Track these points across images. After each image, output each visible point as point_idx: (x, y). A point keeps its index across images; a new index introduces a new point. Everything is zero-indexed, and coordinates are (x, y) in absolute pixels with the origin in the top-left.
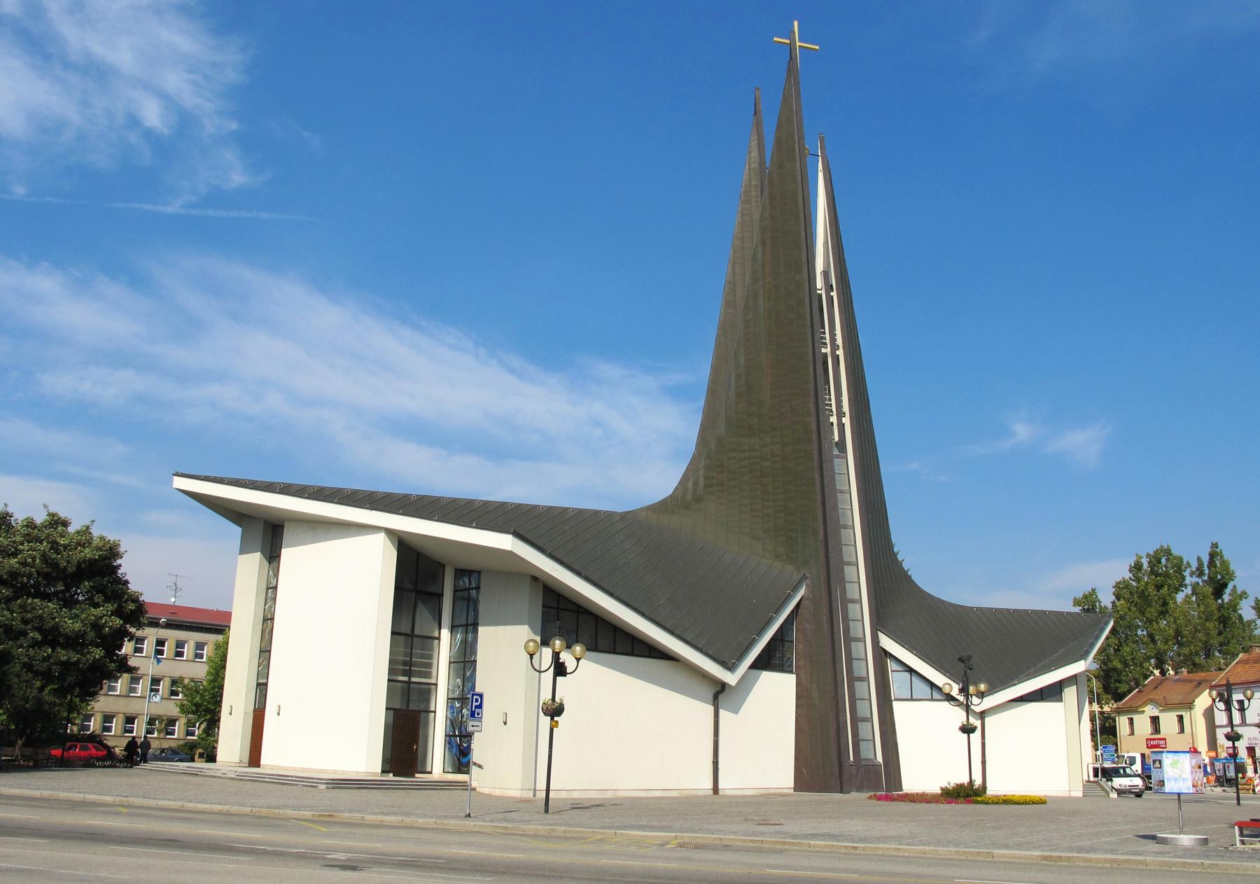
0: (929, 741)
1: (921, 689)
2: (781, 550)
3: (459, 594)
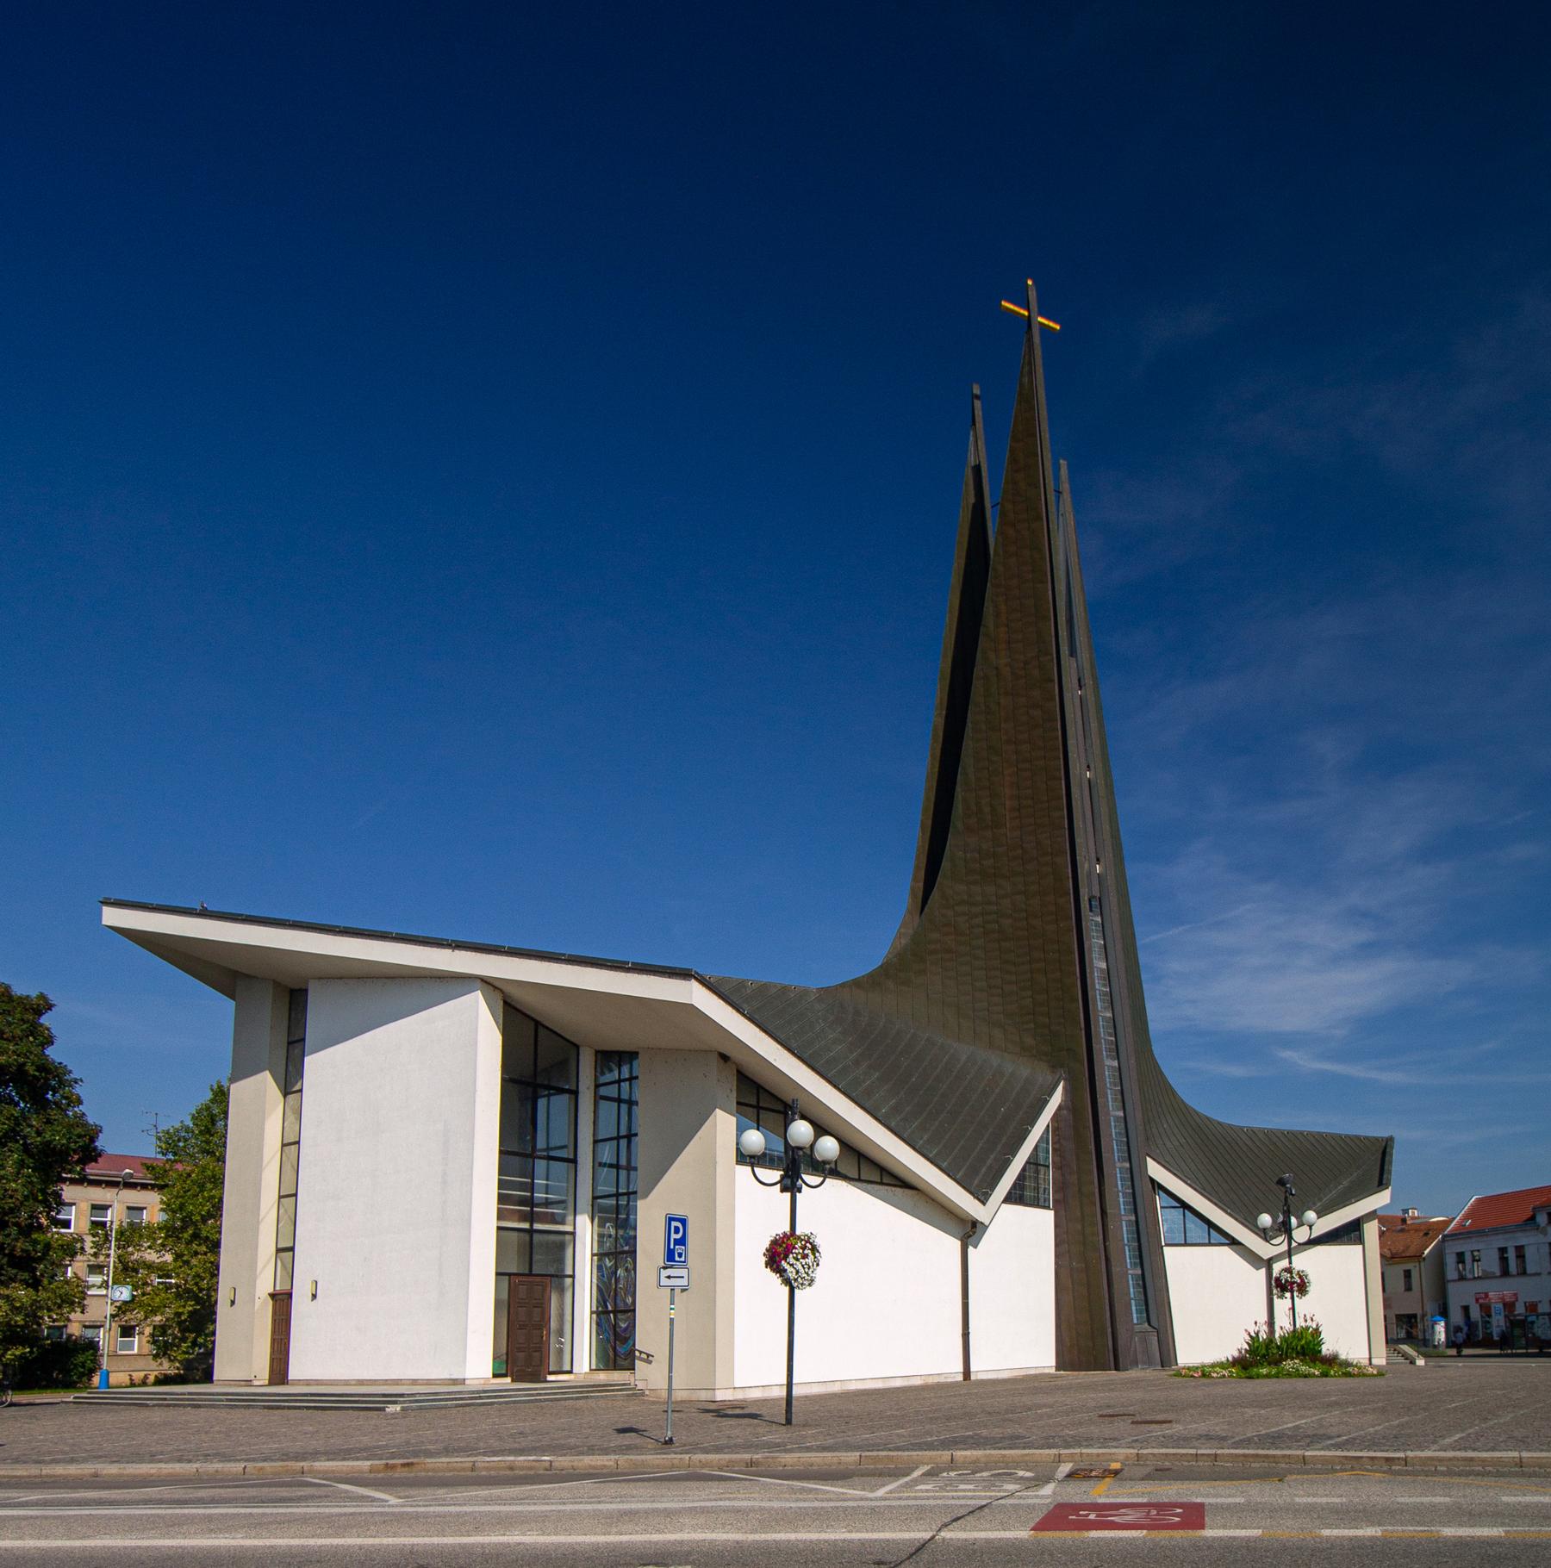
0: (1213, 1300)
1: (1196, 1230)
2: (1029, 1041)
3: (603, 1091)
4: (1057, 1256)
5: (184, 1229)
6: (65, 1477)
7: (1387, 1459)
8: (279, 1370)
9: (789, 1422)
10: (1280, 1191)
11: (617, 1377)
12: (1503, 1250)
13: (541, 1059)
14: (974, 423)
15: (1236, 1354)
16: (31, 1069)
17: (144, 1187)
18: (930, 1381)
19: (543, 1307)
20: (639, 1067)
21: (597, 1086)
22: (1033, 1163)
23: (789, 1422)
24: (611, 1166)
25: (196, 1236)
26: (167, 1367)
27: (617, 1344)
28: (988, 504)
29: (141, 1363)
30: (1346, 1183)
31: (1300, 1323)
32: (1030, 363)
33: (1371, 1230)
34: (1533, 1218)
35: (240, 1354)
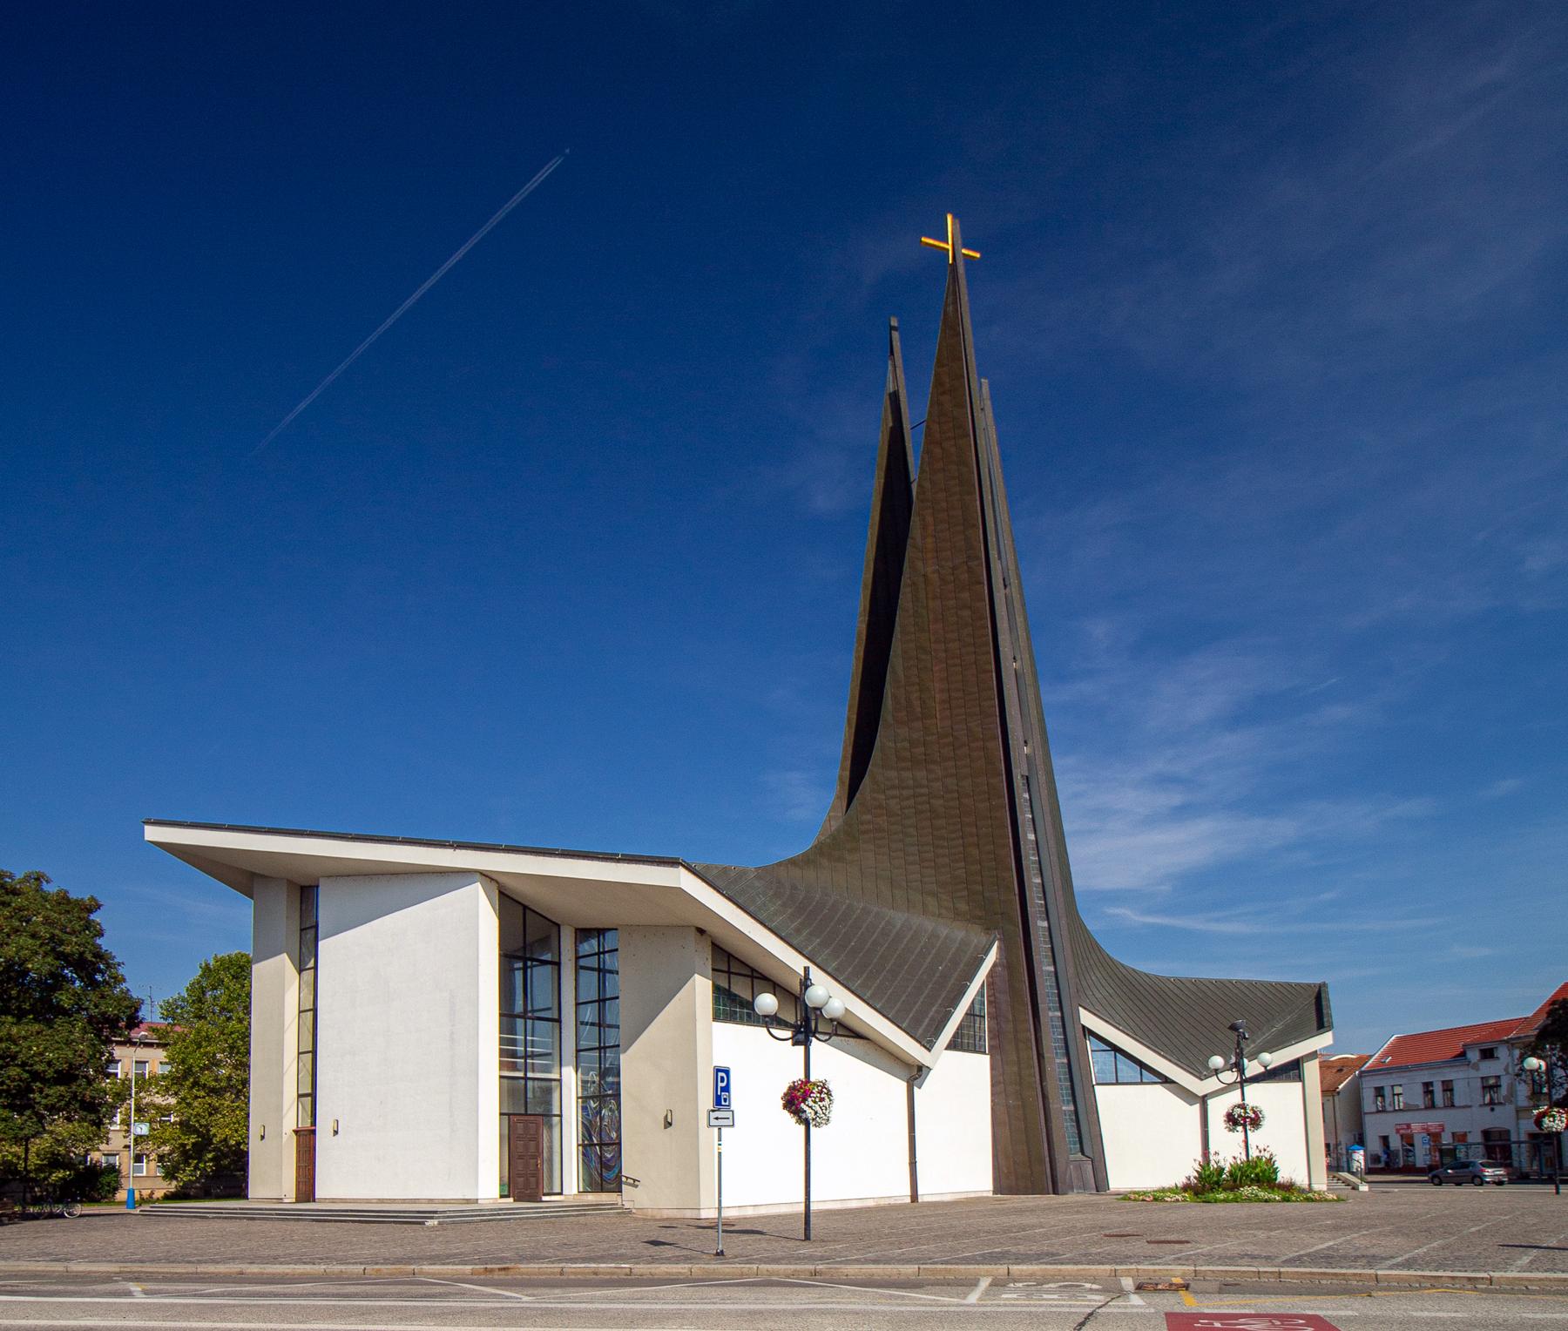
0: (1149, 1134)
2: (963, 907)
3: (582, 962)
4: (993, 1094)
5: (185, 1078)
6: (217, 1274)
7: (1469, 1279)
8: (306, 1187)
9: (807, 1237)
10: (1233, 1035)
11: (604, 1198)
12: (1428, 1087)
13: (529, 935)
16: (89, 957)
17: (150, 1045)
18: (882, 1202)
19: (536, 1139)
20: (610, 941)
21: (577, 958)
22: (971, 1014)
23: (807, 1237)
24: (593, 1024)
25: (196, 1084)
26: (172, 1186)
27: (604, 1168)
28: (907, 426)
29: (149, 1183)
30: (1279, 1026)
31: (1254, 1153)
32: (954, 293)
33: (1312, 1070)
34: (1463, 1054)
35: (271, 1177)
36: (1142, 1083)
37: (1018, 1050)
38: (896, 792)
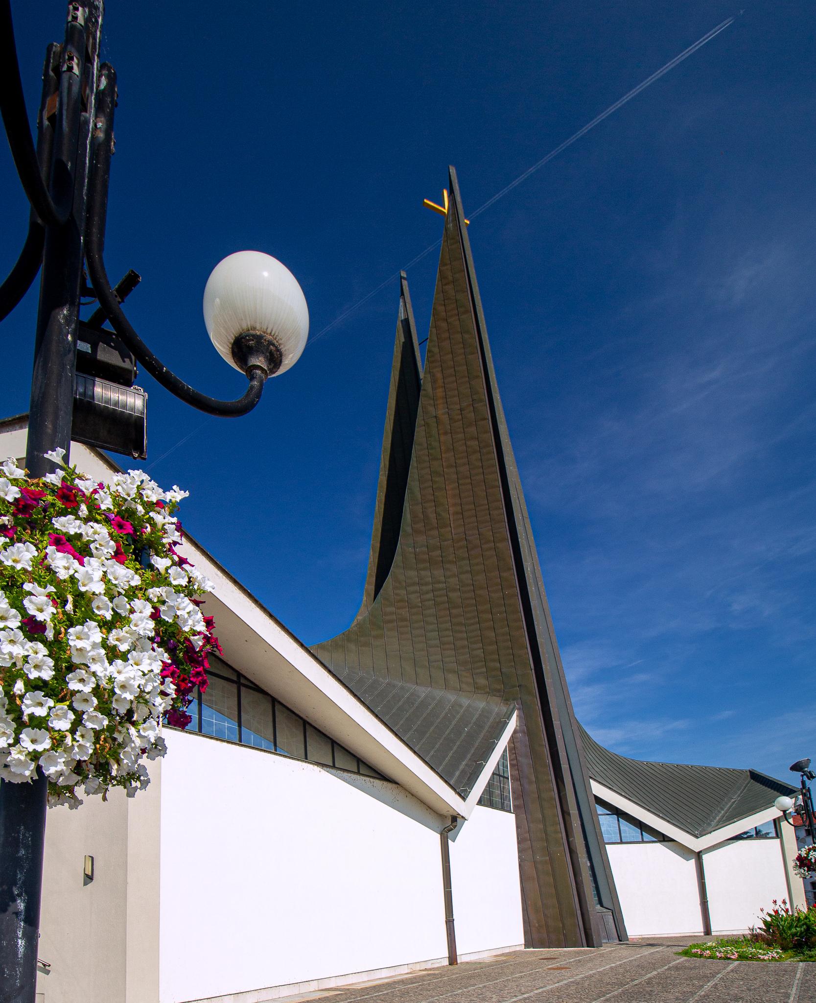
0: (656, 889)
2: (482, 681)
4: (520, 851)
14: (402, 294)
15: (747, 932)
36: (643, 842)
37: (542, 807)
38: (417, 588)
